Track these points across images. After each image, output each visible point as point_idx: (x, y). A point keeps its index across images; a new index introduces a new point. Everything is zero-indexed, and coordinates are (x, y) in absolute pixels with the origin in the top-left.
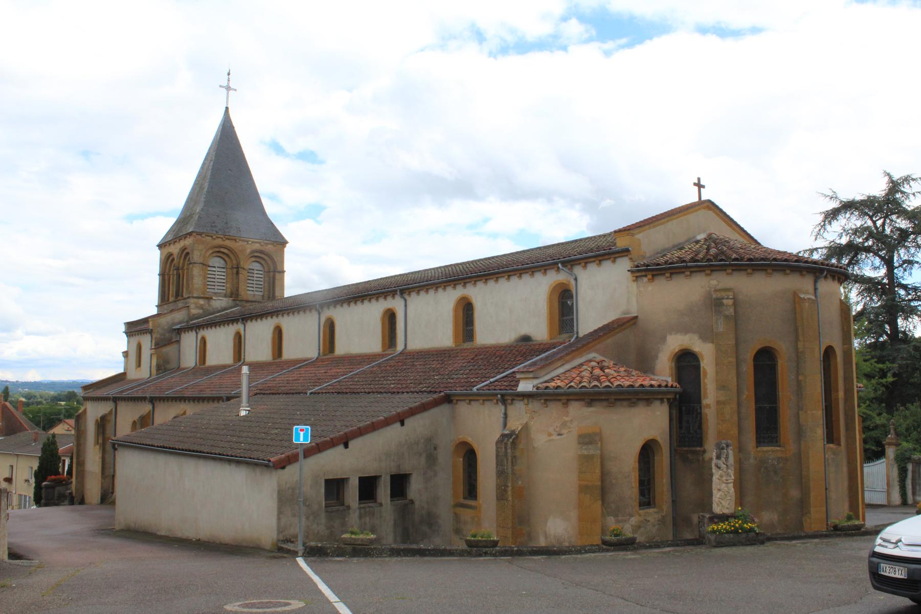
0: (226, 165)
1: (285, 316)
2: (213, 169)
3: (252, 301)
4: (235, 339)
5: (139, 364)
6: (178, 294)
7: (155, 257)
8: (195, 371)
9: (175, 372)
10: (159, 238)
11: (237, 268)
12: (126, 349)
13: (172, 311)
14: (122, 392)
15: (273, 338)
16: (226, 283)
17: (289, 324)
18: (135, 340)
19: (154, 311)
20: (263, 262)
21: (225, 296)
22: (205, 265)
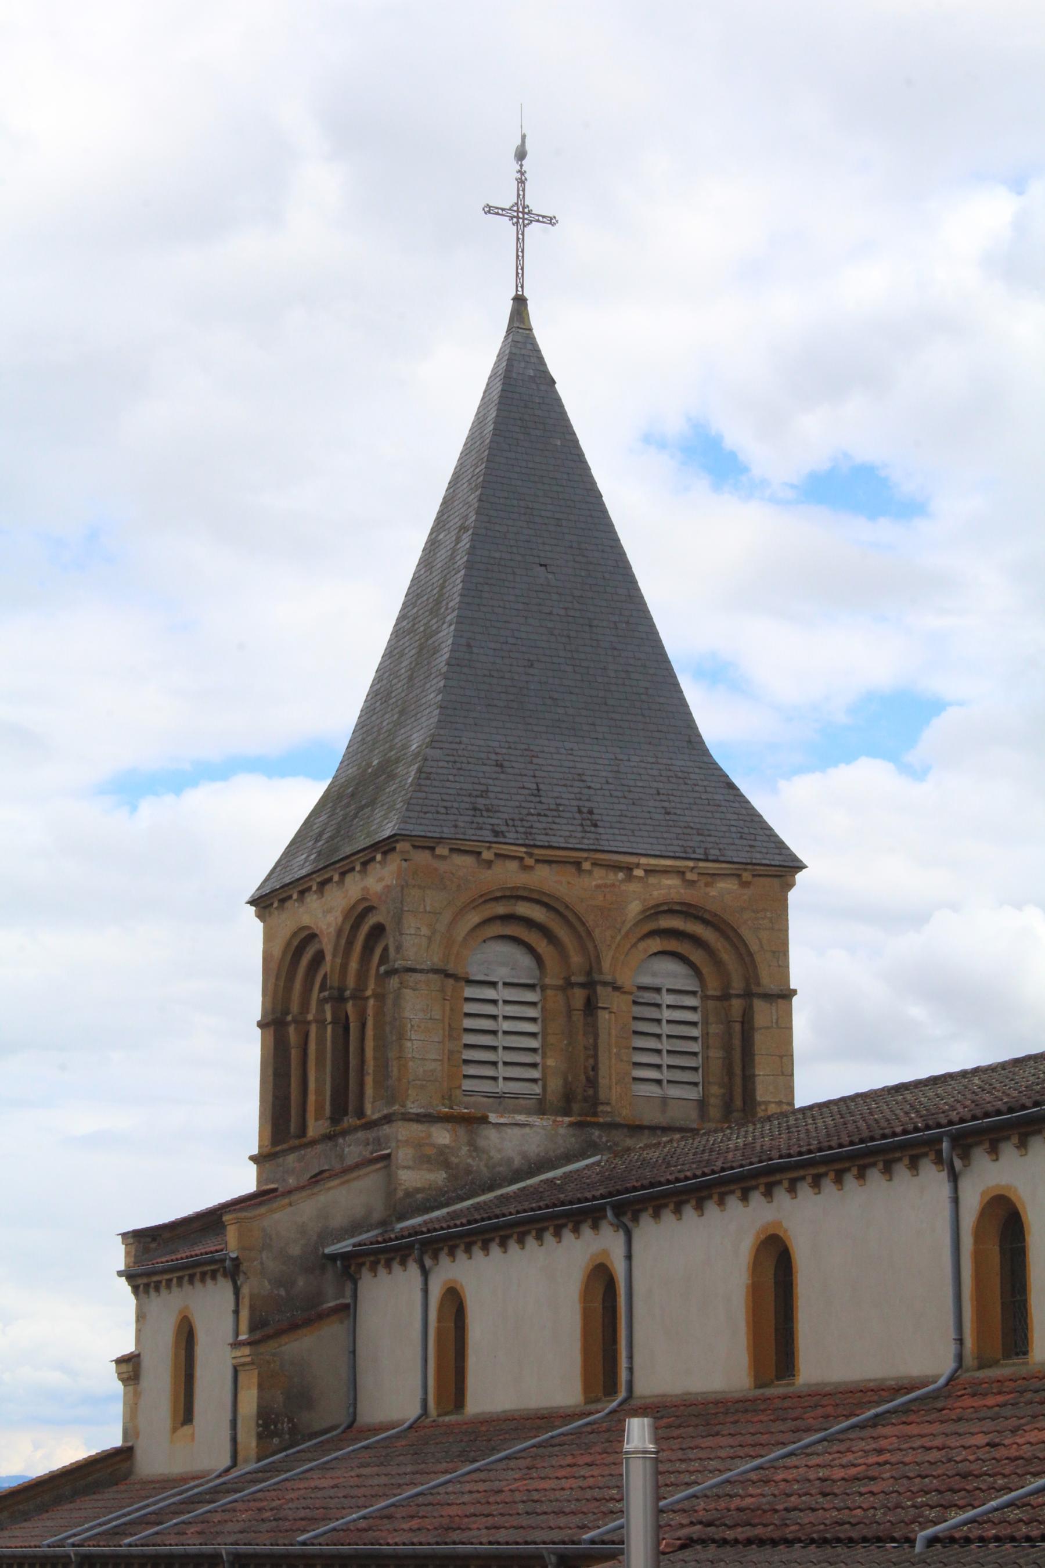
0: (526, 546)
1: (804, 1190)
2: (470, 566)
3: (653, 1129)
4: (586, 1294)
5: (185, 1413)
6: (344, 1104)
7: (243, 945)
8: (419, 1440)
9: (337, 1443)
10: (257, 866)
11: (590, 985)
12: (128, 1347)
13: (317, 1179)
14: (118, 1532)
15: (755, 1290)
16: (544, 1050)
17: (820, 1222)
18: (168, 1306)
19: (245, 1180)
20: (697, 956)
21: (541, 1108)
22: (450, 976)
